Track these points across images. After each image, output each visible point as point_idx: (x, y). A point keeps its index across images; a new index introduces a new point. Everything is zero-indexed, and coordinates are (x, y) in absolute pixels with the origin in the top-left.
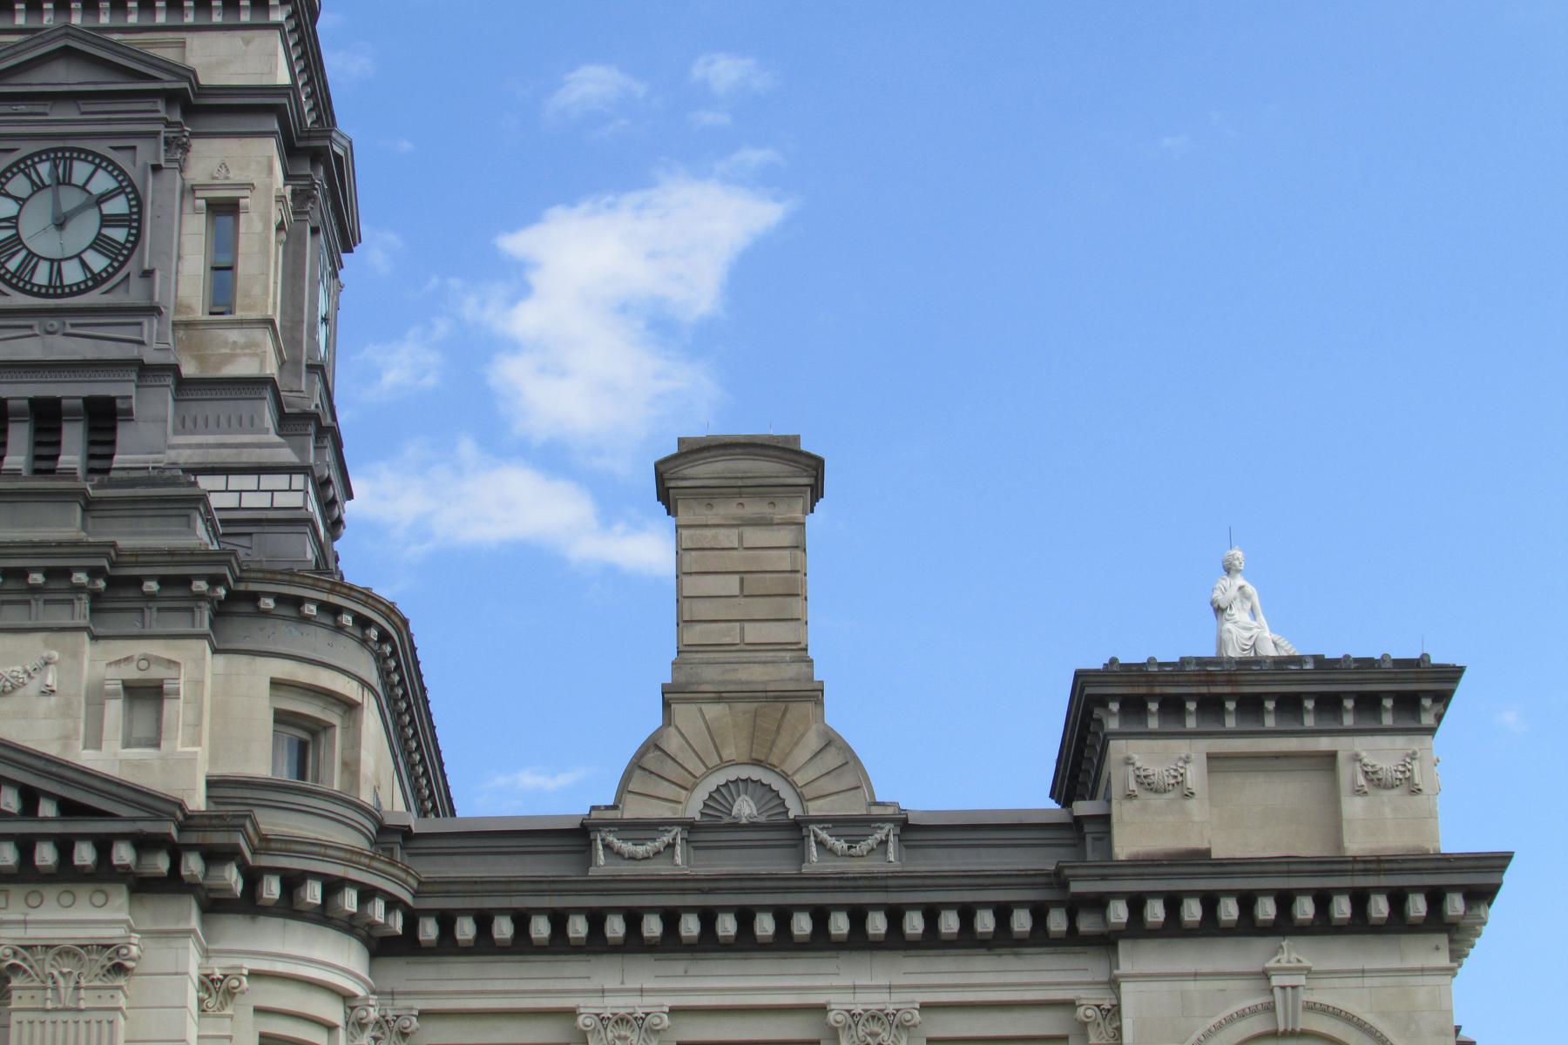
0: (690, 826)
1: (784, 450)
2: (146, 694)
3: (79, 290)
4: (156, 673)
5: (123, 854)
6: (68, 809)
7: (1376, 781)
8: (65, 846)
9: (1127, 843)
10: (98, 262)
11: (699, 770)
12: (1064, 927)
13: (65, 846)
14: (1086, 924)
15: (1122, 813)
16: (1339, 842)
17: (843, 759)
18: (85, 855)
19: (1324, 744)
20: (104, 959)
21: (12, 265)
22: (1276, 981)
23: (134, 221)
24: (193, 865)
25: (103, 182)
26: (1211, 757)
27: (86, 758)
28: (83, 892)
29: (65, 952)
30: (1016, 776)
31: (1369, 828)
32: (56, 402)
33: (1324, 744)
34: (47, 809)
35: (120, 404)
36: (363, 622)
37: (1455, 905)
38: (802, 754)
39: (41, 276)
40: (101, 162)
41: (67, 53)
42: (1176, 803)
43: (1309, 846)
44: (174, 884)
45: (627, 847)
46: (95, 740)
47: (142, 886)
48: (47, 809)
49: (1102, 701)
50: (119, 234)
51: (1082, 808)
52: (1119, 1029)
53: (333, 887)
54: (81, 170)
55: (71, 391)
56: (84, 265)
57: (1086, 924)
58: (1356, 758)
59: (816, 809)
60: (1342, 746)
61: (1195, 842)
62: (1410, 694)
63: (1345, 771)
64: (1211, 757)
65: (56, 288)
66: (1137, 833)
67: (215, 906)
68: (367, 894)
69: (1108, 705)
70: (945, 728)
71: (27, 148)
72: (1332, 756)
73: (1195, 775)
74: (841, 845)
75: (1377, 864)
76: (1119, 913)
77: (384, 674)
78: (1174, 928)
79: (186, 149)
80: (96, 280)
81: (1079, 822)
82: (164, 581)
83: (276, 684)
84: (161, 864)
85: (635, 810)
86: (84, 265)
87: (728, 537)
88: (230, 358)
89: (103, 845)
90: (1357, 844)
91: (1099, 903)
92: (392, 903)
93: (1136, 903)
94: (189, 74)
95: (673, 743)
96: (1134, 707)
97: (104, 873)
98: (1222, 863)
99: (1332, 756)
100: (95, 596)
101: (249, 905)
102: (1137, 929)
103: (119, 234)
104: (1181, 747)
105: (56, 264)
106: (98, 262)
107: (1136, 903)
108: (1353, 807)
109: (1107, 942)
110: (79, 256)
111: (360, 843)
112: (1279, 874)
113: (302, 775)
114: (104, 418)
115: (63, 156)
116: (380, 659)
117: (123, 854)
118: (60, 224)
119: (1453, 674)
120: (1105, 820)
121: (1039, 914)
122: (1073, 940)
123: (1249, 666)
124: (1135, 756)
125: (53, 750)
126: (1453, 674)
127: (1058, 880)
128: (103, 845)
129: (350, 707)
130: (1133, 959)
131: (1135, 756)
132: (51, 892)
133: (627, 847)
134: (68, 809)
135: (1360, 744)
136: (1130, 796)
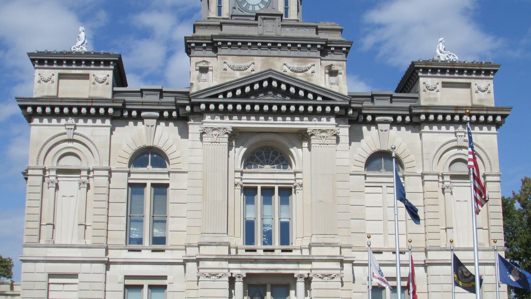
6: (324, 98)
8: (324, 107)
12: (190, 110)
13: (324, 107)
15: (422, 94)
18: (328, 109)
19: (468, 81)
21: (244, 6)
22: (458, 134)
26: (443, 83)
56: (259, 7)
57: (415, 120)
60: (91, 72)
73: (439, 87)
86: (259, 7)
89: (333, 107)
104: (53, 71)
110: (258, 4)
112: (494, 110)
127: (410, 109)
128: (333, 107)
134: (324, 98)
135: (477, 81)
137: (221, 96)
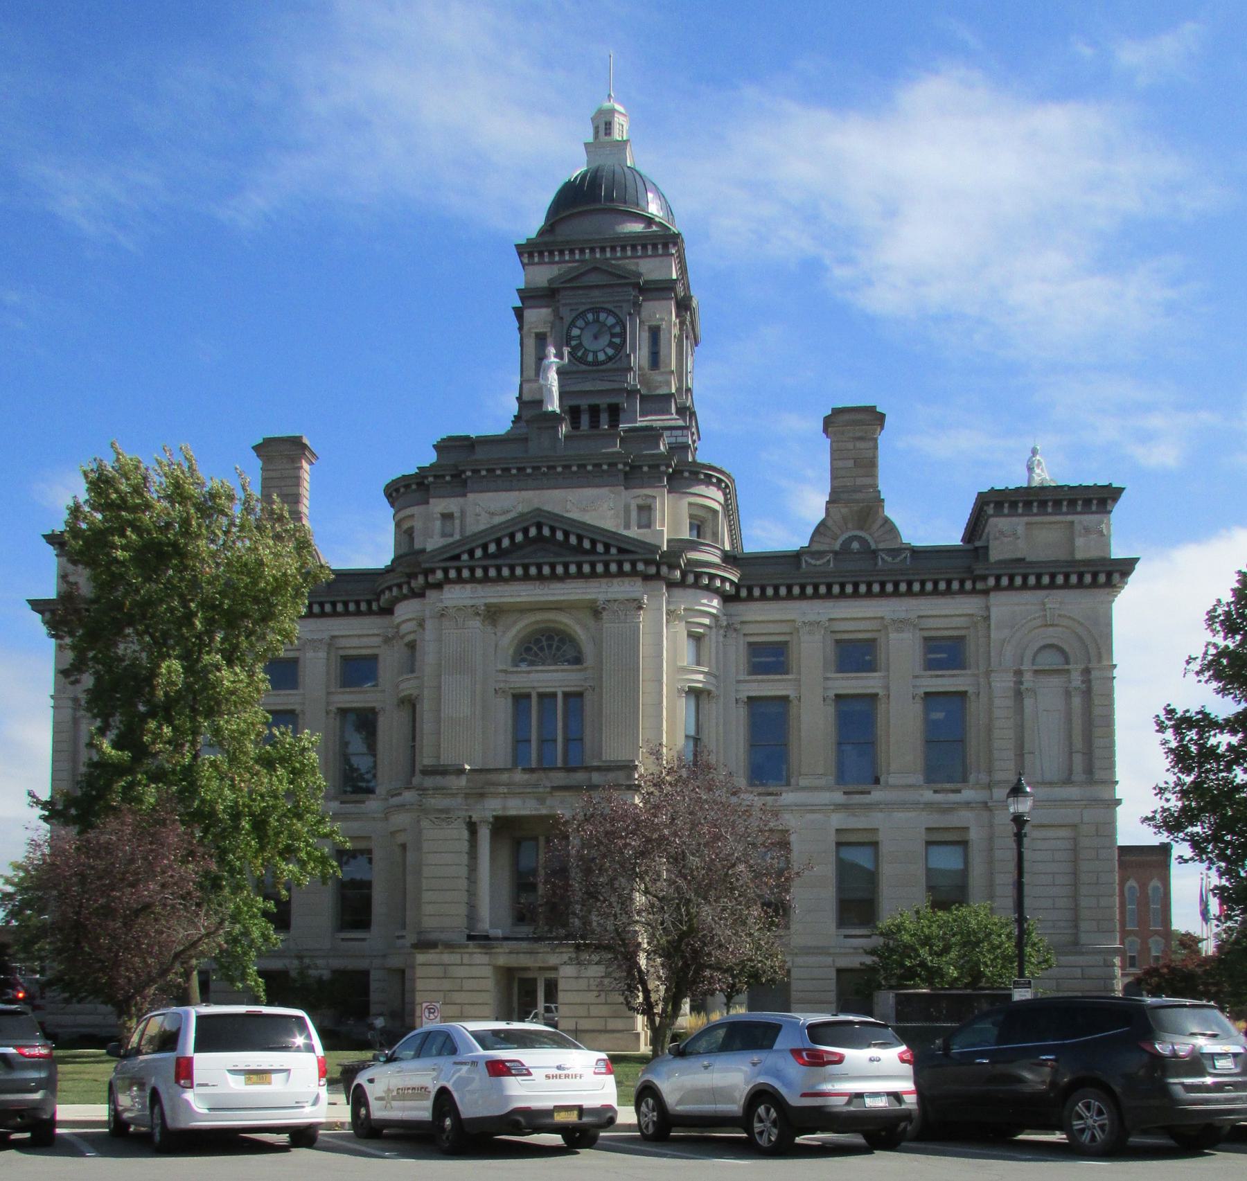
0: (836, 553)
1: (871, 410)
2: (646, 510)
3: (603, 363)
4: (649, 501)
5: (640, 567)
6: (621, 551)
7: (1087, 530)
9: (994, 555)
10: (610, 352)
11: (839, 532)
14: (979, 586)
16: (1072, 552)
17: (890, 528)
20: (635, 604)
23: (622, 335)
24: (664, 570)
25: (611, 321)
27: (626, 533)
28: (627, 580)
29: (622, 602)
30: (950, 534)
31: (1084, 549)
32: (598, 406)
33: (1069, 518)
34: (613, 551)
35: (92, 476)
36: (720, 481)
37: (1116, 577)
38: (876, 526)
39: (590, 358)
40: (610, 312)
41: (595, 269)
42: (1013, 538)
43: (1062, 555)
44: (657, 576)
45: (813, 562)
46: (627, 526)
47: (646, 578)
48: (613, 551)
49: (987, 504)
50: (617, 340)
51: (978, 544)
52: (989, 626)
53: (712, 577)
54: (603, 316)
55: (603, 401)
57: (979, 586)
58: (1080, 522)
59: (881, 546)
61: (1019, 555)
62: (1102, 498)
63: (1078, 527)
64: (1027, 524)
65: (596, 363)
66: (998, 552)
67: (671, 585)
68: (724, 579)
69: (990, 505)
70: (927, 519)
71: (582, 308)
72: (1072, 523)
74: (890, 559)
75: (1087, 562)
76: (991, 582)
77: (726, 500)
78: (1011, 586)
79: (640, 305)
80: (610, 359)
81: (976, 549)
82: (650, 467)
83: (690, 504)
84: (652, 570)
85: (816, 547)
87: (850, 446)
88: (657, 388)
89: (634, 565)
90: (1079, 556)
91: (984, 578)
92: (732, 582)
93: (998, 578)
94: (639, 275)
95: (830, 523)
96: (999, 505)
97: (634, 573)
98: (1030, 563)
99: (1072, 523)
100: (626, 474)
101: (682, 584)
102: (998, 587)
103: (617, 340)
104: (1015, 519)
105: (595, 353)
106: (610, 352)
107: (998, 578)
108: (1079, 542)
109: (986, 592)
111: (718, 560)
113: (699, 536)
114: (615, 412)
115: (596, 311)
116: (725, 495)
117: (640, 567)
118: (596, 337)
119: (1120, 491)
120: (986, 548)
121: (962, 583)
122: (974, 591)
123: (1043, 489)
124: (998, 524)
125: (614, 530)
126: (1120, 491)
128: (634, 565)
129: (715, 512)
130: (995, 598)
131: (998, 524)
132: (616, 581)
133: (813, 562)
134: (621, 551)
136: (996, 539)
137: (465, 557)
